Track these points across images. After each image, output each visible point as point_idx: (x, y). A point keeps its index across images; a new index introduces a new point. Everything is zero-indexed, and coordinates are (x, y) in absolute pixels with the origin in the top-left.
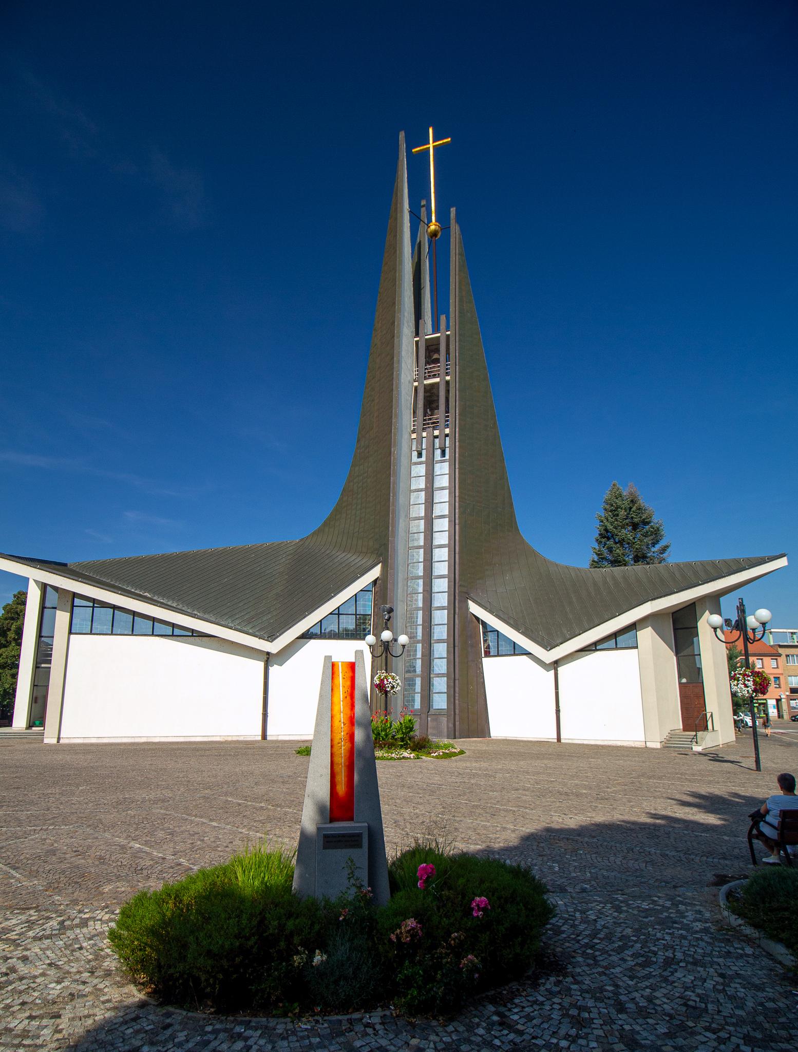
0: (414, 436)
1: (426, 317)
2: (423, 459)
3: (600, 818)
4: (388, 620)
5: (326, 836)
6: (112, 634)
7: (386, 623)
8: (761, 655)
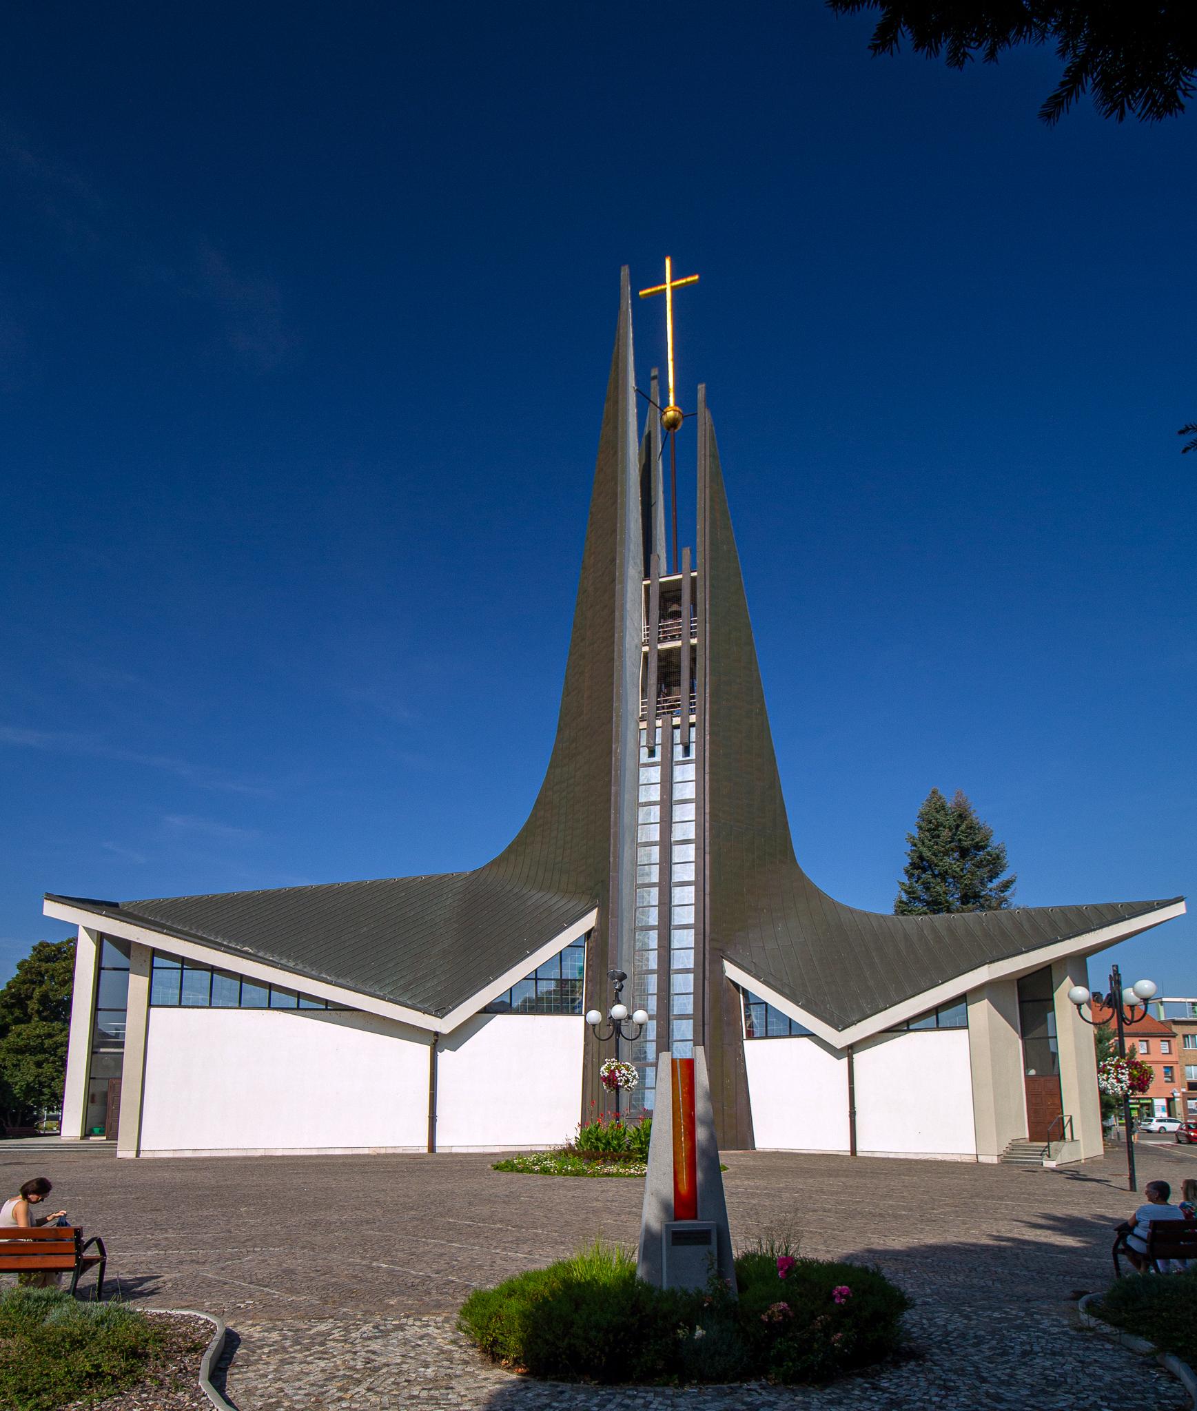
0: (643, 725)
1: (659, 548)
2: (658, 758)
3: (930, 1240)
4: (620, 990)
5: (674, 1233)
6: (210, 1007)
7: (617, 995)
8: (1145, 1035)
